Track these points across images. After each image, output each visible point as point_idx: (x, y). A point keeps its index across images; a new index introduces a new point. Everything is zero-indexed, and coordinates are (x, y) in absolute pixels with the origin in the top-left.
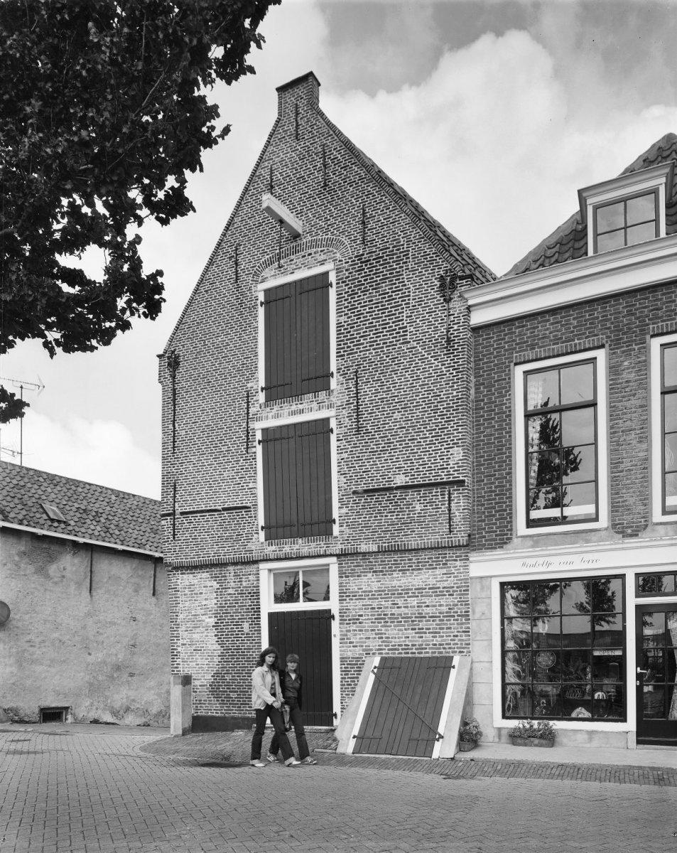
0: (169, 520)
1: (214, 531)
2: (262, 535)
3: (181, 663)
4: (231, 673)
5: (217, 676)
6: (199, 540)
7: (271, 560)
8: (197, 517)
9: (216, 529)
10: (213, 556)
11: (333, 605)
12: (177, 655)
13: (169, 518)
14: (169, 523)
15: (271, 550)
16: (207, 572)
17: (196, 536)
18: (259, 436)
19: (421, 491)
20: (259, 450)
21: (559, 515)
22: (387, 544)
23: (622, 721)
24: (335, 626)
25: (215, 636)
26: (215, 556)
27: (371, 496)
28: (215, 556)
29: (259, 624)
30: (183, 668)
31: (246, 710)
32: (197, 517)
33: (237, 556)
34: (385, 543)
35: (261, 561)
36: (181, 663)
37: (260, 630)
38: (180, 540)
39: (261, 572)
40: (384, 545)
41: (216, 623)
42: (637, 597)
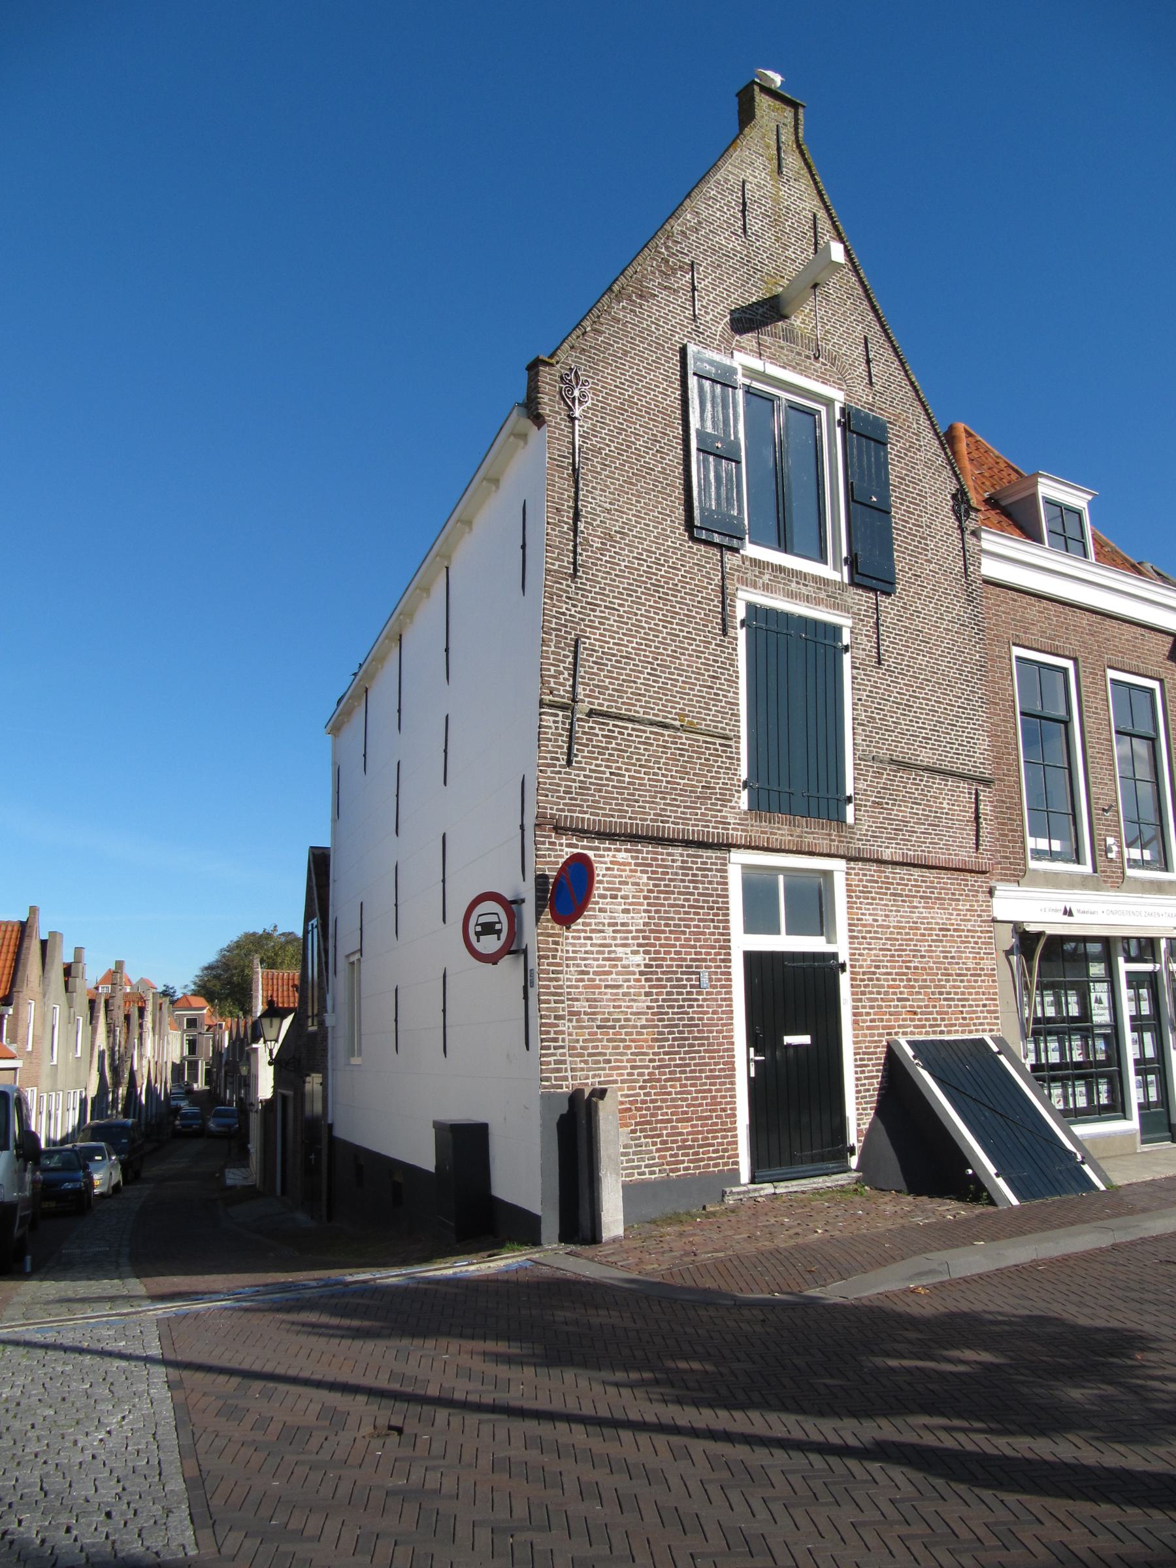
0: (560, 719)
1: (659, 768)
2: (743, 800)
3: (568, 1059)
4: (680, 1079)
5: (652, 1087)
6: (627, 779)
7: (757, 848)
8: (627, 728)
9: (665, 764)
10: (693, 825)
11: (842, 948)
12: (555, 1040)
13: (561, 713)
14: (560, 725)
15: (759, 830)
16: (627, 851)
17: (619, 768)
18: (741, 613)
19: (948, 781)
20: (742, 634)
21: (1139, 857)
22: (912, 853)
23: (1125, 1118)
24: (844, 979)
25: (647, 994)
26: (656, 821)
27: (603, 724)
28: (656, 821)
29: (729, 973)
30: (572, 1070)
31: (710, 1159)
32: (627, 728)
33: (586, 816)
34: (910, 850)
35: (738, 847)
36: (568, 1059)
37: (730, 986)
38: (584, 769)
39: (730, 867)
40: (909, 853)
41: (646, 966)
42: (778, 933)
